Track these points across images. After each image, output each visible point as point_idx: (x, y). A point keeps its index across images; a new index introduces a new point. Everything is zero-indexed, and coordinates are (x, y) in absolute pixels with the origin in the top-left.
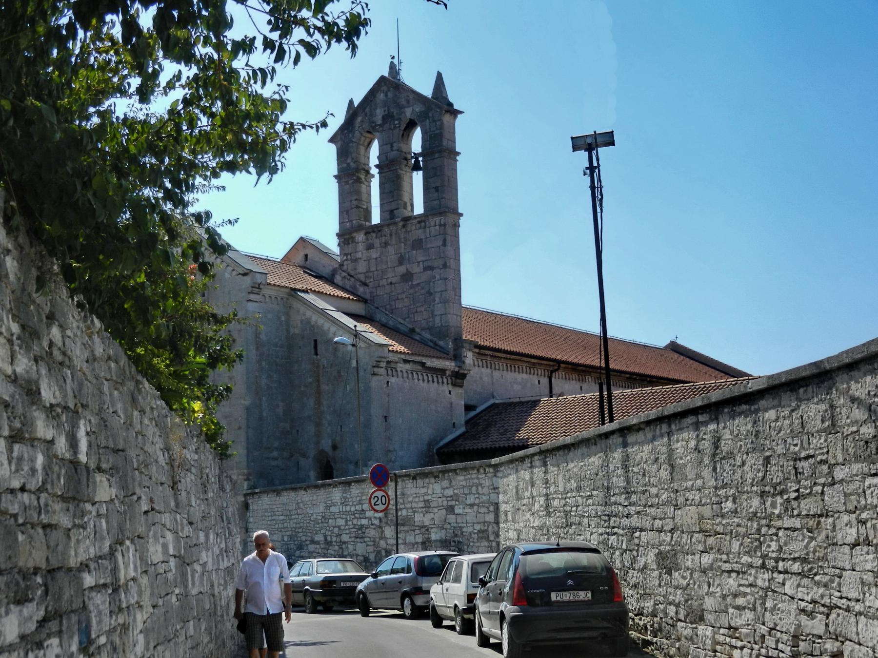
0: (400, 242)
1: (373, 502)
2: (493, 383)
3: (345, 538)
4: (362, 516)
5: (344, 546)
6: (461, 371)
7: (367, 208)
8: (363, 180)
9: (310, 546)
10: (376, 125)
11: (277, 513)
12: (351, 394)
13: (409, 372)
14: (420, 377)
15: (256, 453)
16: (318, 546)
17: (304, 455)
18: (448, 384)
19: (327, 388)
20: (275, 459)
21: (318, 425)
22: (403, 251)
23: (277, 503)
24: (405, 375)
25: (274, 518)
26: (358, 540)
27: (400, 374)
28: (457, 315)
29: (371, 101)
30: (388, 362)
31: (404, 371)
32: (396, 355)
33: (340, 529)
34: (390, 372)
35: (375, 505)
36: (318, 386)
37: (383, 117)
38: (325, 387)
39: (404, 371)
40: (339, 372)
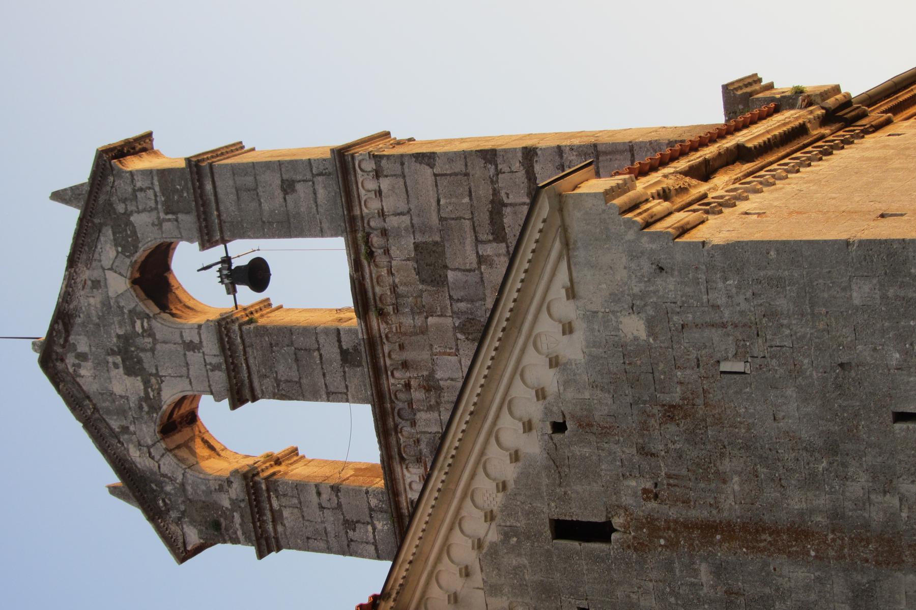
0: (424, 331)
10: (147, 398)
12: (758, 347)
22: (449, 321)
29: (96, 409)
36: (728, 530)
40: (671, 412)
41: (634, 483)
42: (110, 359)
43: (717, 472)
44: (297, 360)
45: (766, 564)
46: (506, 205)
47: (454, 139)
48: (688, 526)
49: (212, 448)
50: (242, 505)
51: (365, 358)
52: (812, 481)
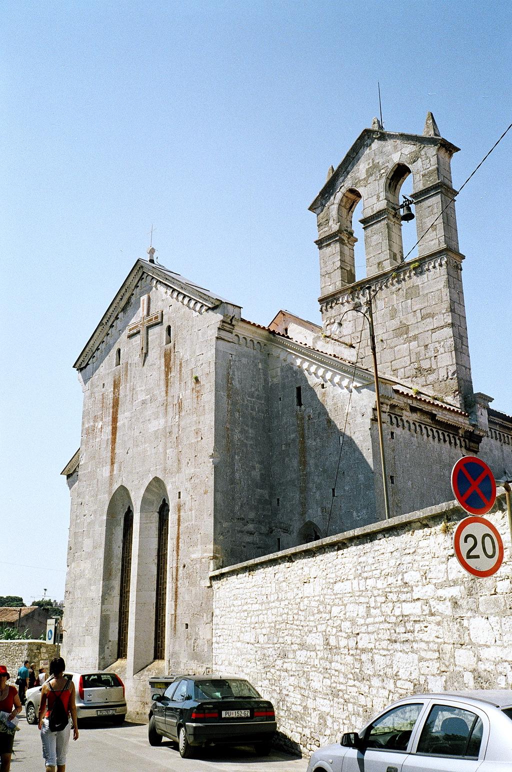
1: (464, 548)
2: (504, 459)
3: (364, 642)
4: (403, 597)
5: (364, 657)
6: (477, 432)
7: (351, 270)
8: (346, 242)
9: (298, 653)
11: (249, 601)
13: (417, 424)
14: (430, 433)
15: (225, 525)
16: (313, 654)
17: (286, 530)
18: (461, 446)
19: (314, 443)
20: (251, 534)
21: (304, 490)
23: (248, 585)
24: (412, 427)
25: (245, 608)
26: (397, 646)
27: (406, 425)
28: (466, 368)
30: (393, 407)
31: (411, 422)
32: (401, 398)
33: (353, 622)
34: (394, 420)
35: (469, 557)
36: (303, 443)
37: (367, 171)
38: (311, 443)
39: (411, 422)
41: (311, 412)
42: (371, 161)
43: (316, 438)
44: (378, 244)
45: (297, 454)
46: (433, 319)
47: (214, 501)
48: (303, 430)
49: (351, 208)
50: (330, 230)
51: (381, 272)
52: (316, 466)
